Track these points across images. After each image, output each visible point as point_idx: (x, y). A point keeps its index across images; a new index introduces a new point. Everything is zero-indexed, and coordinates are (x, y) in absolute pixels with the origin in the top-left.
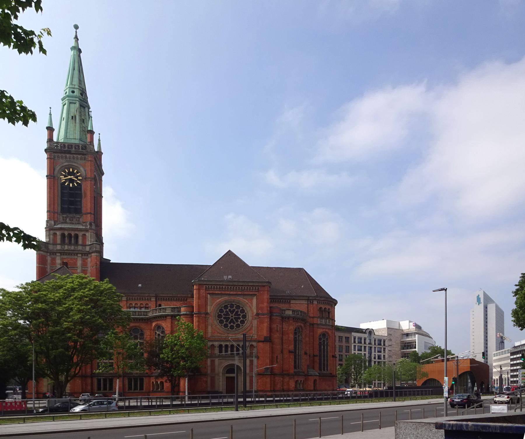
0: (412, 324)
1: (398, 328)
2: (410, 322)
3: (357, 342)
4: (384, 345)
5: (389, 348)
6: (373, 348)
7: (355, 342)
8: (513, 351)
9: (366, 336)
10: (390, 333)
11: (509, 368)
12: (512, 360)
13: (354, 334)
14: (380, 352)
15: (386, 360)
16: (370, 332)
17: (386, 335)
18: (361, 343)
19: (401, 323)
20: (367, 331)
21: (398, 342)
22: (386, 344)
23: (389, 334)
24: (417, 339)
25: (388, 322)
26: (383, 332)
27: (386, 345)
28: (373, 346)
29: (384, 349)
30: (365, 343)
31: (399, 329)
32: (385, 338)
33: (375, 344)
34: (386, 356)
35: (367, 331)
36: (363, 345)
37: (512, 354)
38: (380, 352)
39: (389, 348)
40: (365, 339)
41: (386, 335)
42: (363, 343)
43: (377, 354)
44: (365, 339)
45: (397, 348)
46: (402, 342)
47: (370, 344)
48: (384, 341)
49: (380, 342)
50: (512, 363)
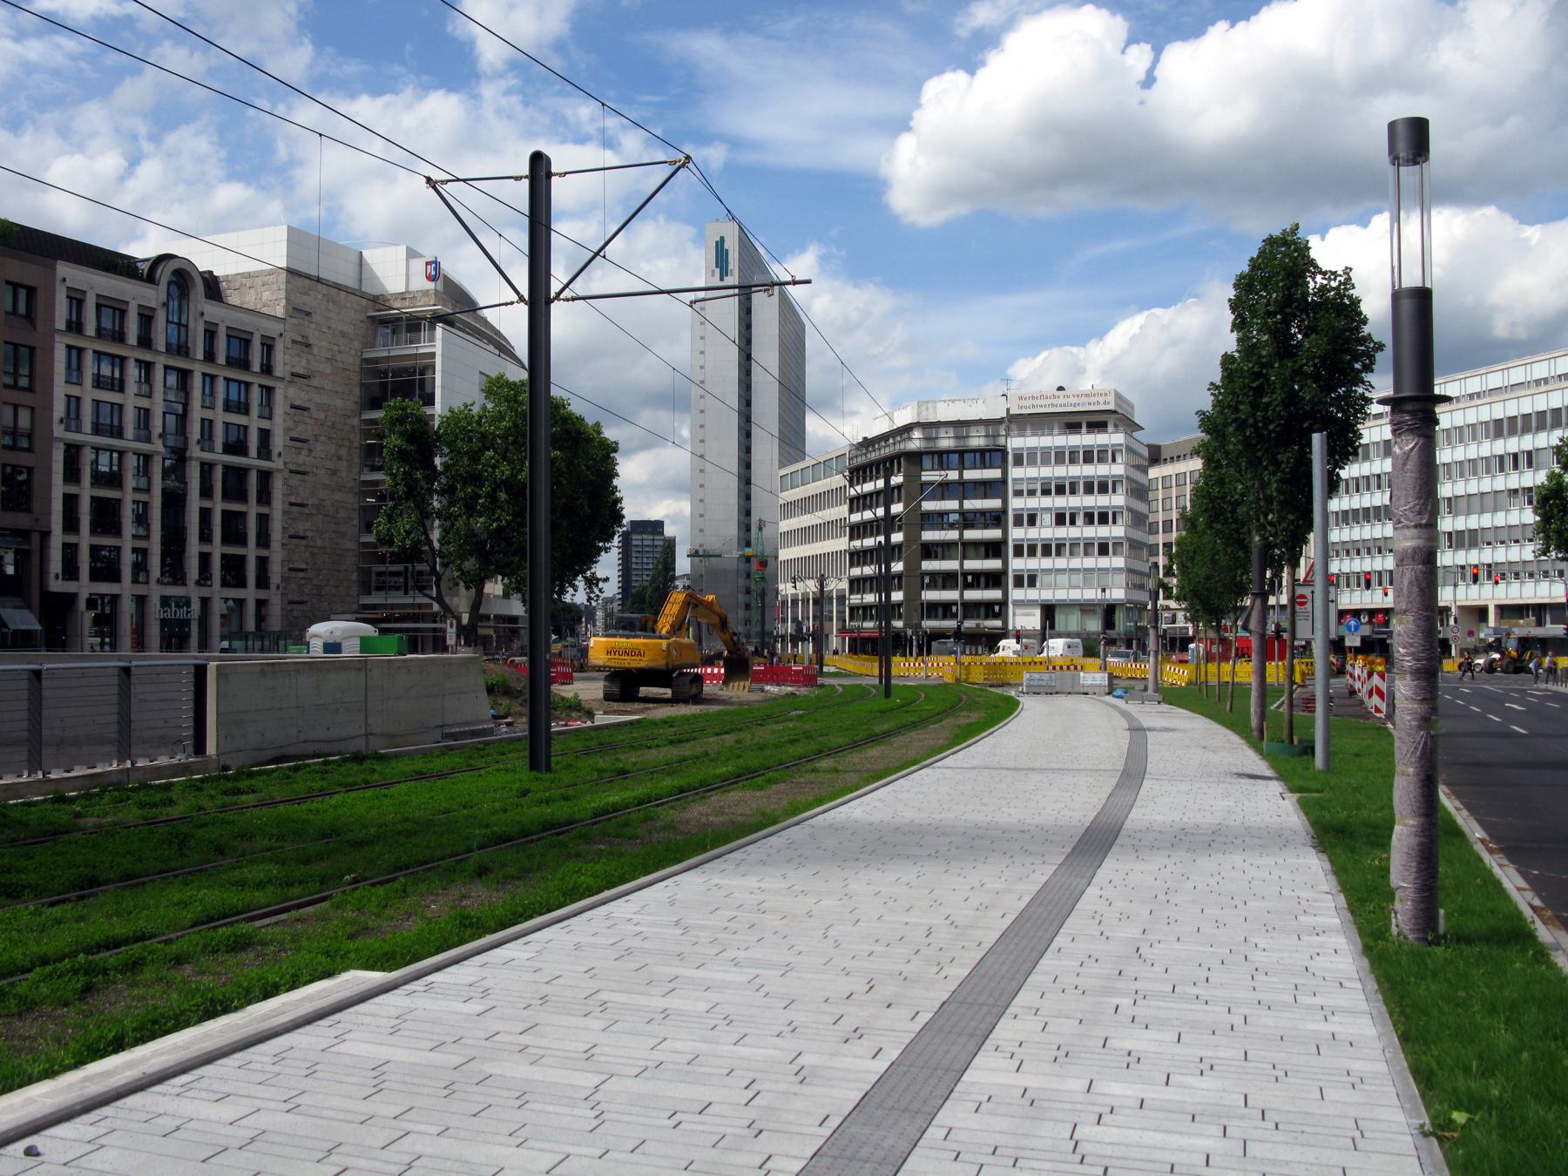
0: (418, 266)
1: (351, 283)
2: (412, 254)
3: (221, 359)
4: (267, 369)
5: (296, 394)
6: (197, 381)
7: (75, 326)
8: (861, 460)
9: (152, 296)
10: (308, 302)
11: (841, 543)
12: (857, 503)
13: (64, 269)
14: (244, 409)
15: (276, 464)
16: (180, 279)
17: (280, 311)
18: (244, 365)
19: (365, 253)
20: (164, 274)
21: (350, 360)
22: (283, 362)
23: (297, 311)
24: (438, 349)
25: (296, 238)
26: (266, 295)
27: (279, 370)
28: (198, 370)
29: (268, 391)
30: (145, 341)
31: (357, 293)
32: (273, 329)
33: (210, 356)
34: (278, 442)
35: (164, 274)
36: (85, 539)
37: (858, 473)
38: (244, 409)
39: (296, 394)
40: (146, 318)
41: (280, 311)
42: (132, 338)
43: (220, 417)
44: (146, 318)
45: (337, 396)
46: (371, 367)
47: (182, 350)
48: (268, 346)
49: (243, 348)
50: (856, 518)
